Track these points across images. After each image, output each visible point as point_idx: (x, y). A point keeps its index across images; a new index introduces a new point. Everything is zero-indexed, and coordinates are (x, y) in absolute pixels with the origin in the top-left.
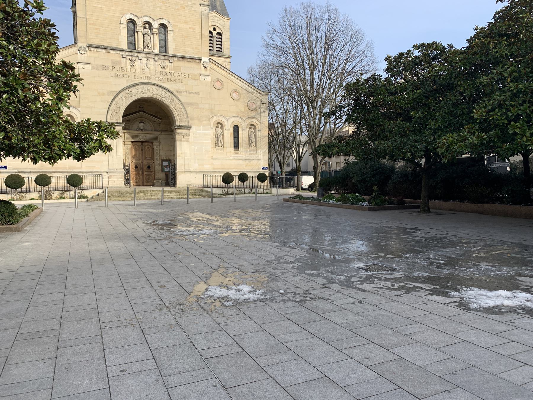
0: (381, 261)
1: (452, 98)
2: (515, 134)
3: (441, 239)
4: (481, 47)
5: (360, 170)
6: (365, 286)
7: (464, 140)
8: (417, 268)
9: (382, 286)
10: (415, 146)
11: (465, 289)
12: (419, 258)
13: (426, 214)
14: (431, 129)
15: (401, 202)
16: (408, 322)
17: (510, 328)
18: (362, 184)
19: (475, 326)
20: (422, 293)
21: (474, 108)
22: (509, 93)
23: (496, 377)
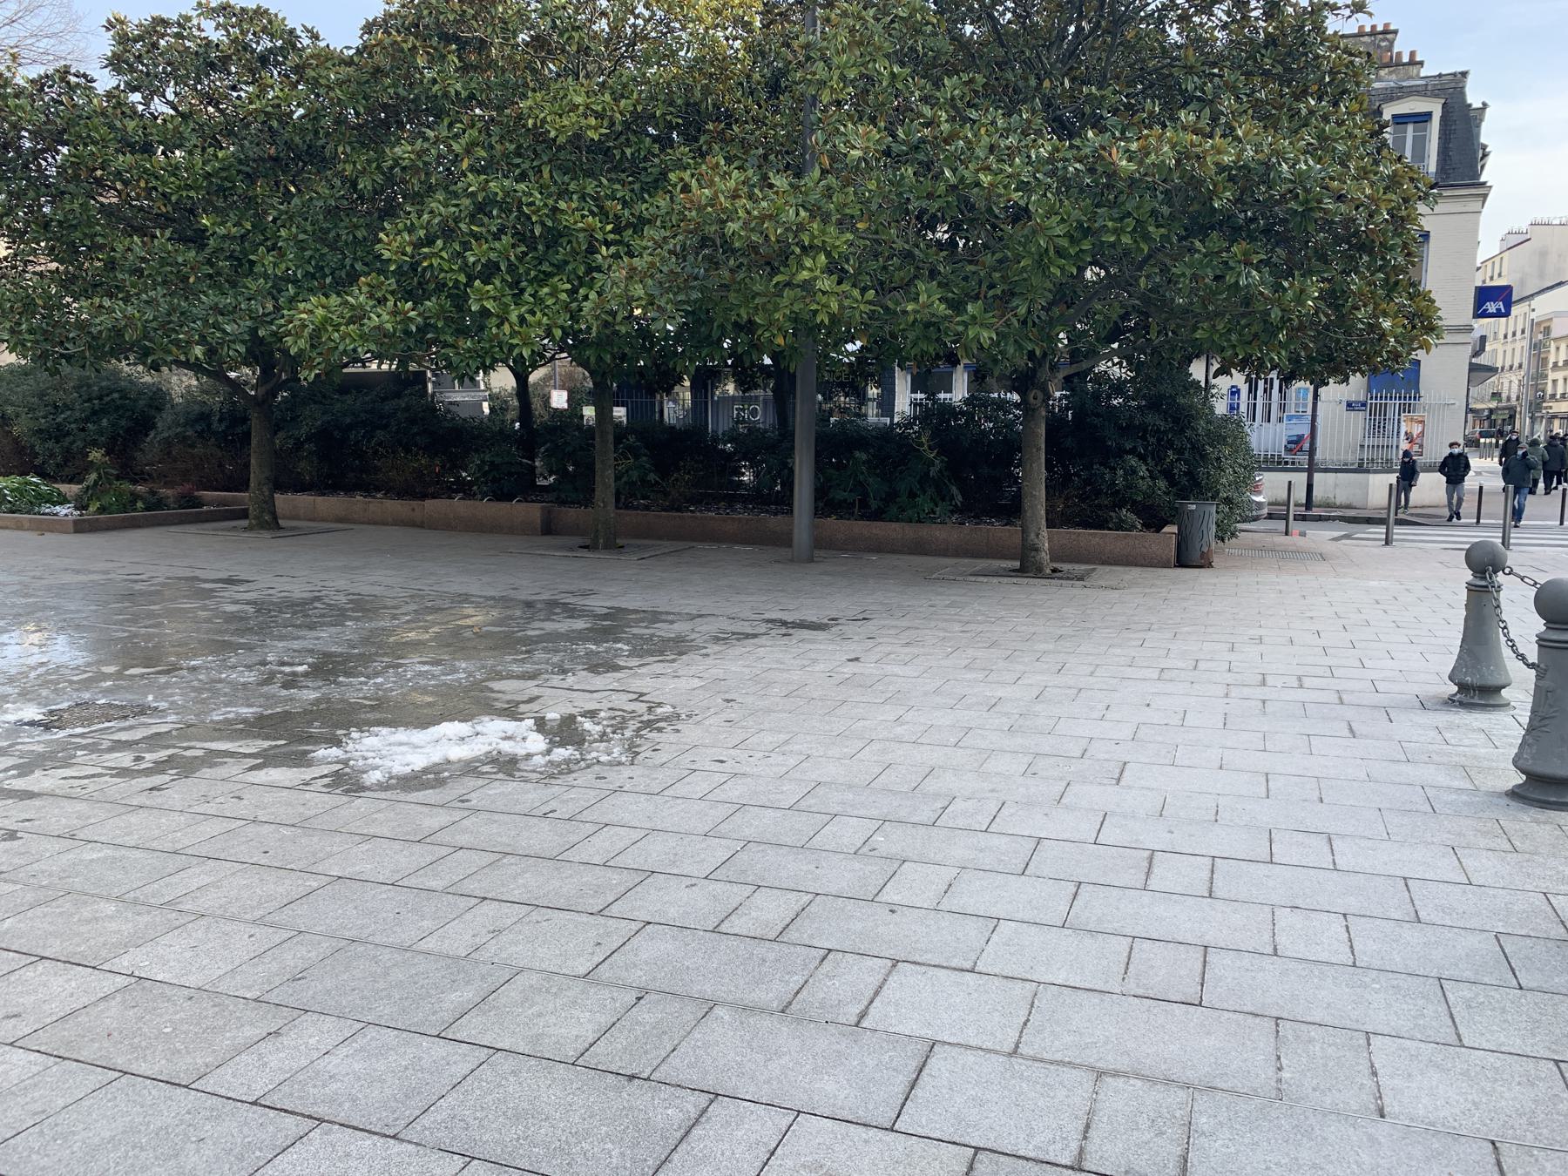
0: (106, 692)
1: (323, 191)
2: (485, 313)
3: (304, 603)
4: (393, 57)
5: (42, 395)
6: (39, 781)
7: (358, 317)
8: (225, 695)
9: (99, 770)
10: (216, 326)
11: (355, 735)
12: (234, 667)
13: (266, 534)
14: (266, 276)
15: (191, 502)
16: (174, 863)
17: (457, 815)
18: (50, 444)
19: (372, 832)
20: (232, 769)
21: (383, 229)
22: (466, 202)
23: (408, 954)
